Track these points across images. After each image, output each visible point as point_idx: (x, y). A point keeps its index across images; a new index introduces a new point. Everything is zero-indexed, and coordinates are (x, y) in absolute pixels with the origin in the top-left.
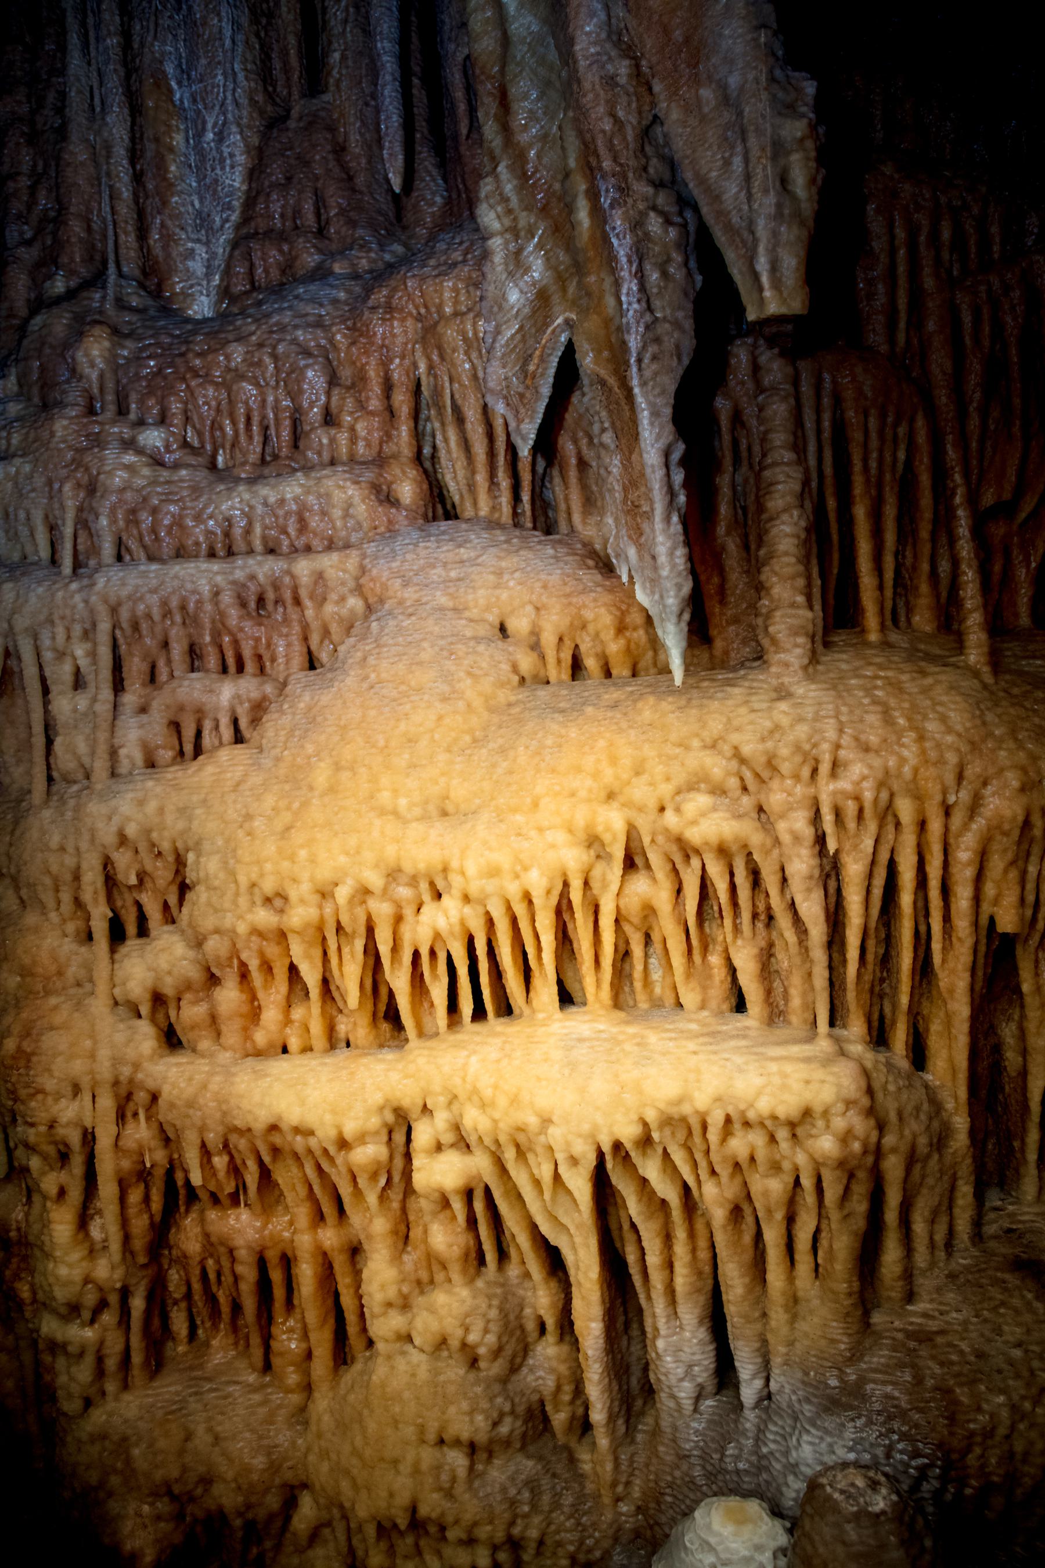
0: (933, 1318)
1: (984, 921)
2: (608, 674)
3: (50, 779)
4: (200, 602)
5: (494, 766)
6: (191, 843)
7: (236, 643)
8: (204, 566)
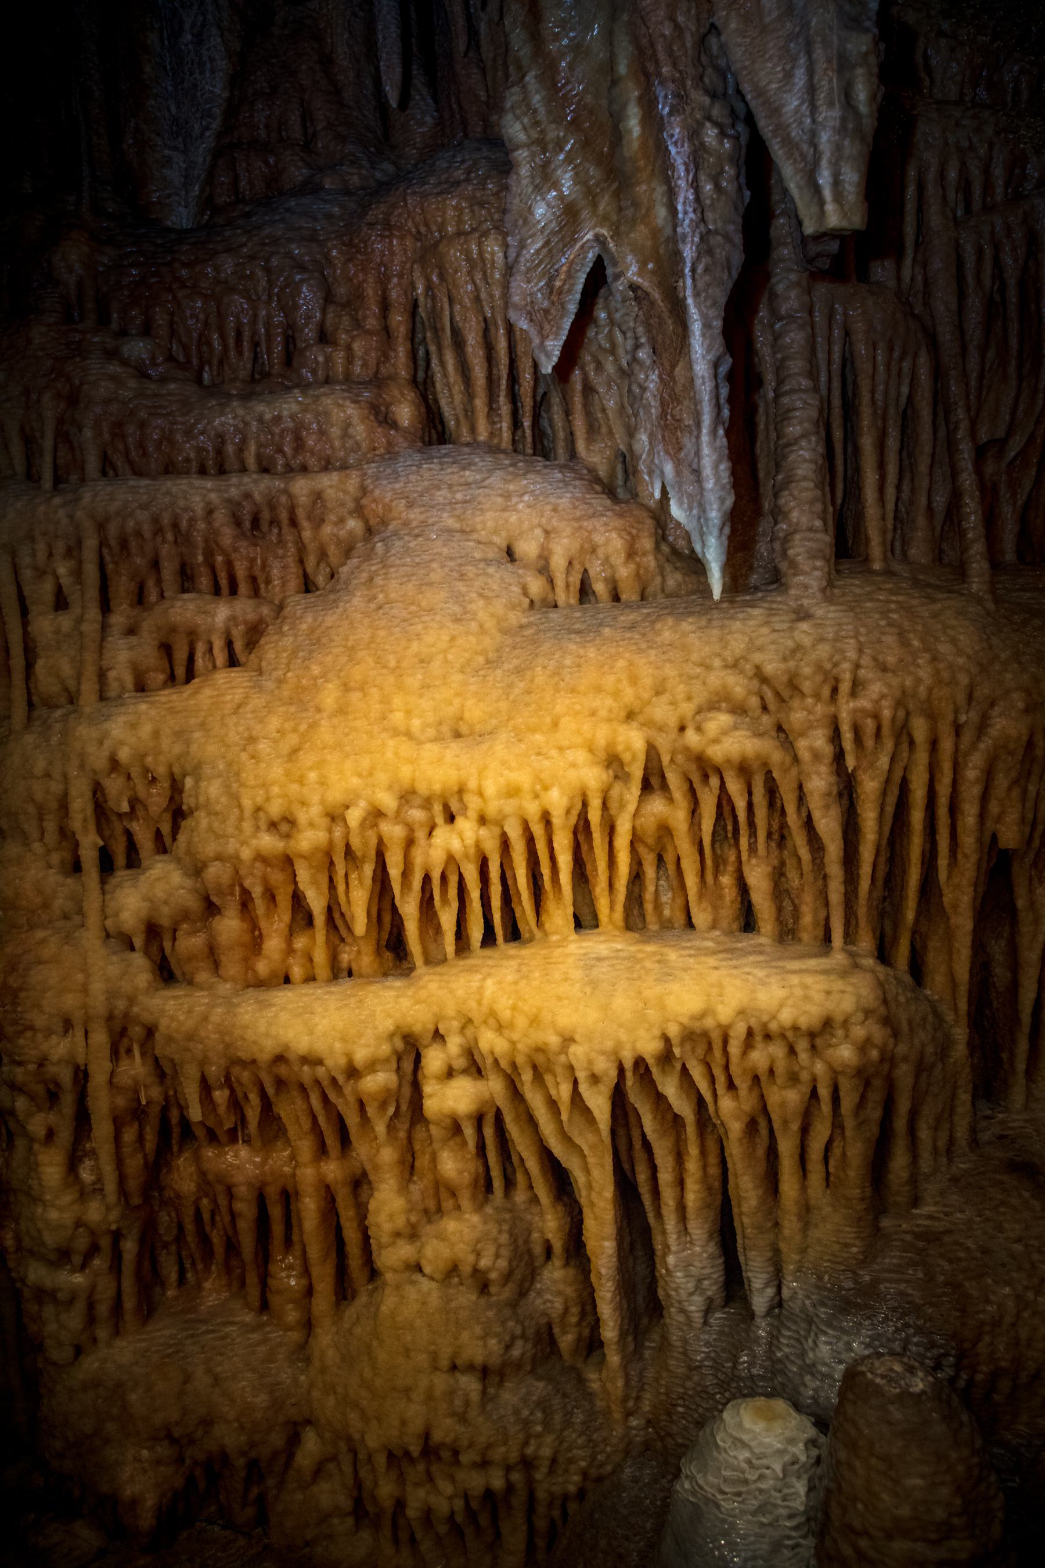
0: (939, 1219)
1: (987, 839)
2: (616, 598)
3: (31, 705)
4: (192, 520)
5: (510, 686)
6: (188, 767)
7: (229, 564)
8: (197, 482)
